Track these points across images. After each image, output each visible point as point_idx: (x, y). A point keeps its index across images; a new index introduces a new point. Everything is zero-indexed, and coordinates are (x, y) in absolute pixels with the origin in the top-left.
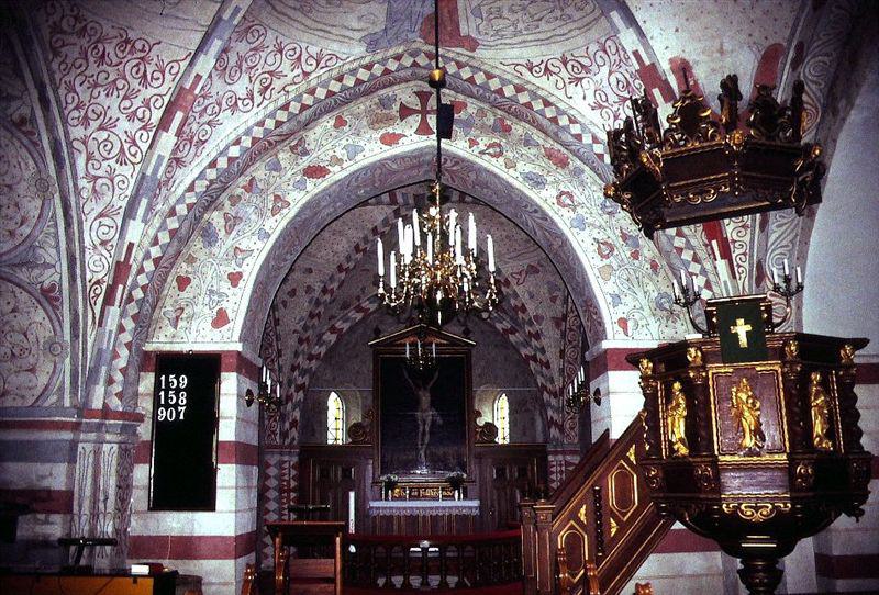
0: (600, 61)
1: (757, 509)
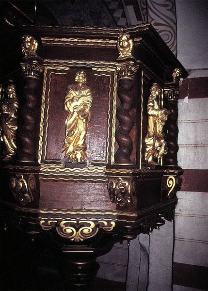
1: (77, 227)
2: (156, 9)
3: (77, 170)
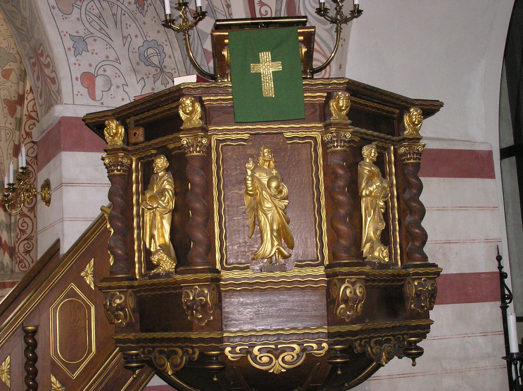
1: (276, 352)
3: (278, 274)
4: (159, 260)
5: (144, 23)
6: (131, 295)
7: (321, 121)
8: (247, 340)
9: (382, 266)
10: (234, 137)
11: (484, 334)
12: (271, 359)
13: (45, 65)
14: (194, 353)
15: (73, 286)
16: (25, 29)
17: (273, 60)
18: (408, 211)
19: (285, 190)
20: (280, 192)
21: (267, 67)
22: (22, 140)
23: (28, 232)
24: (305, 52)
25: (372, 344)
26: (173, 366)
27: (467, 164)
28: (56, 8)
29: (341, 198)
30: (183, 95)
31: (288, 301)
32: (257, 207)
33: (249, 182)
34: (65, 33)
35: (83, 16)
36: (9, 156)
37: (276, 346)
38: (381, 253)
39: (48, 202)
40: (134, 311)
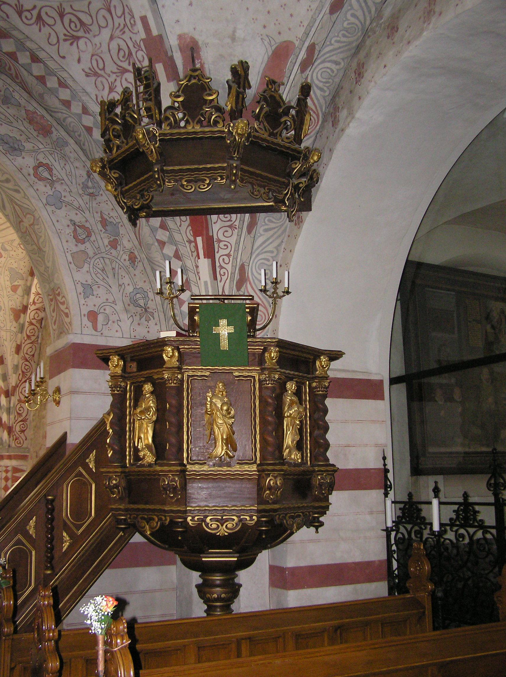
0: (103, 23)
1: (222, 522)
2: (255, 285)
3: (225, 468)
4: (144, 455)
5: (135, 275)
6: (123, 478)
7: (258, 366)
8: (203, 512)
9: (296, 465)
10: (199, 374)
11: (371, 513)
12: (218, 526)
13: (61, 303)
14: (166, 520)
15: (80, 469)
16: (46, 274)
17: (228, 325)
18: (317, 426)
19: (233, 412)
20: (230, 413)
21: (224, 330)
22: (23, 341)
23: (24, 415)
24: (250, 320)
25: (287, 518)
26: (151, 528)
27: (363, 389)
28: (73, 263)
29: (270, 419)
30: (167, 345)
31: (231, 487)
32: (212, 423)
33: (209, 406)
34: (77, 281)
35: (91, 269)
36: (12, 353)
37: (222, 517)
38: (296, 456)
39: (58, 403)
40: (124, 488)
